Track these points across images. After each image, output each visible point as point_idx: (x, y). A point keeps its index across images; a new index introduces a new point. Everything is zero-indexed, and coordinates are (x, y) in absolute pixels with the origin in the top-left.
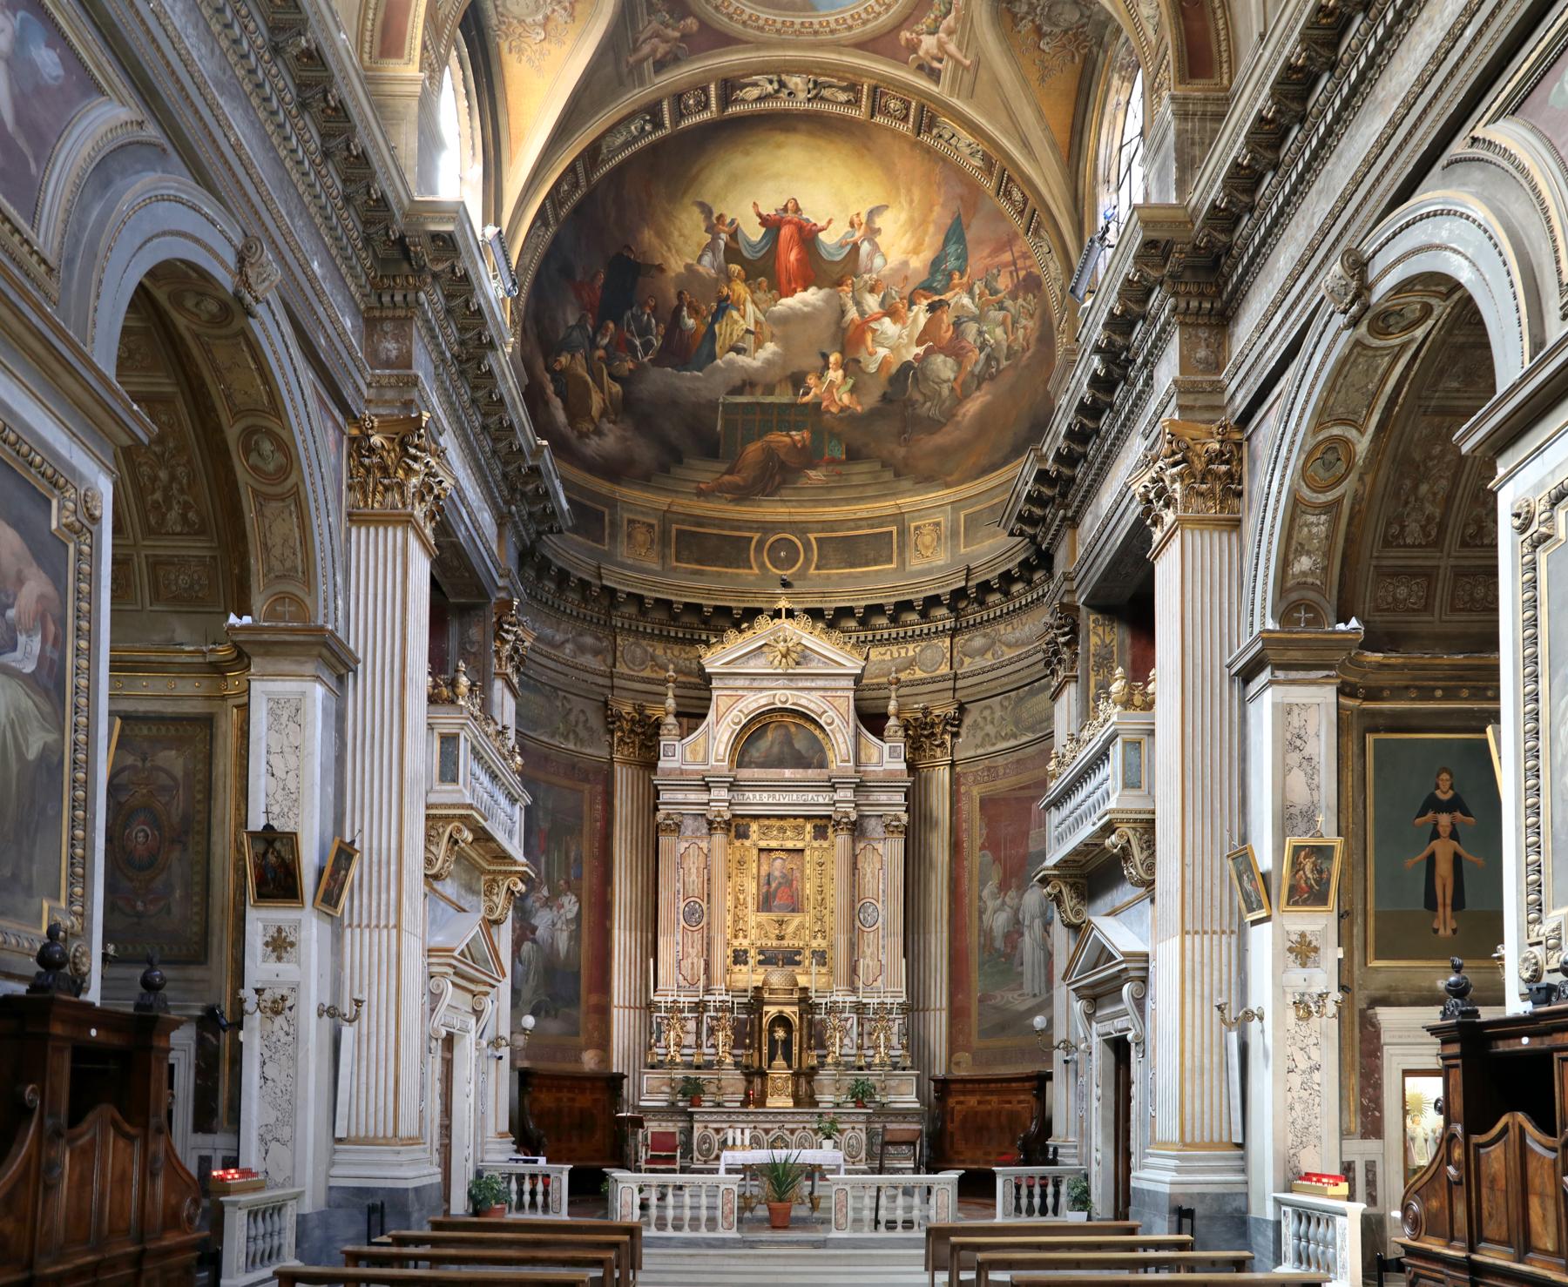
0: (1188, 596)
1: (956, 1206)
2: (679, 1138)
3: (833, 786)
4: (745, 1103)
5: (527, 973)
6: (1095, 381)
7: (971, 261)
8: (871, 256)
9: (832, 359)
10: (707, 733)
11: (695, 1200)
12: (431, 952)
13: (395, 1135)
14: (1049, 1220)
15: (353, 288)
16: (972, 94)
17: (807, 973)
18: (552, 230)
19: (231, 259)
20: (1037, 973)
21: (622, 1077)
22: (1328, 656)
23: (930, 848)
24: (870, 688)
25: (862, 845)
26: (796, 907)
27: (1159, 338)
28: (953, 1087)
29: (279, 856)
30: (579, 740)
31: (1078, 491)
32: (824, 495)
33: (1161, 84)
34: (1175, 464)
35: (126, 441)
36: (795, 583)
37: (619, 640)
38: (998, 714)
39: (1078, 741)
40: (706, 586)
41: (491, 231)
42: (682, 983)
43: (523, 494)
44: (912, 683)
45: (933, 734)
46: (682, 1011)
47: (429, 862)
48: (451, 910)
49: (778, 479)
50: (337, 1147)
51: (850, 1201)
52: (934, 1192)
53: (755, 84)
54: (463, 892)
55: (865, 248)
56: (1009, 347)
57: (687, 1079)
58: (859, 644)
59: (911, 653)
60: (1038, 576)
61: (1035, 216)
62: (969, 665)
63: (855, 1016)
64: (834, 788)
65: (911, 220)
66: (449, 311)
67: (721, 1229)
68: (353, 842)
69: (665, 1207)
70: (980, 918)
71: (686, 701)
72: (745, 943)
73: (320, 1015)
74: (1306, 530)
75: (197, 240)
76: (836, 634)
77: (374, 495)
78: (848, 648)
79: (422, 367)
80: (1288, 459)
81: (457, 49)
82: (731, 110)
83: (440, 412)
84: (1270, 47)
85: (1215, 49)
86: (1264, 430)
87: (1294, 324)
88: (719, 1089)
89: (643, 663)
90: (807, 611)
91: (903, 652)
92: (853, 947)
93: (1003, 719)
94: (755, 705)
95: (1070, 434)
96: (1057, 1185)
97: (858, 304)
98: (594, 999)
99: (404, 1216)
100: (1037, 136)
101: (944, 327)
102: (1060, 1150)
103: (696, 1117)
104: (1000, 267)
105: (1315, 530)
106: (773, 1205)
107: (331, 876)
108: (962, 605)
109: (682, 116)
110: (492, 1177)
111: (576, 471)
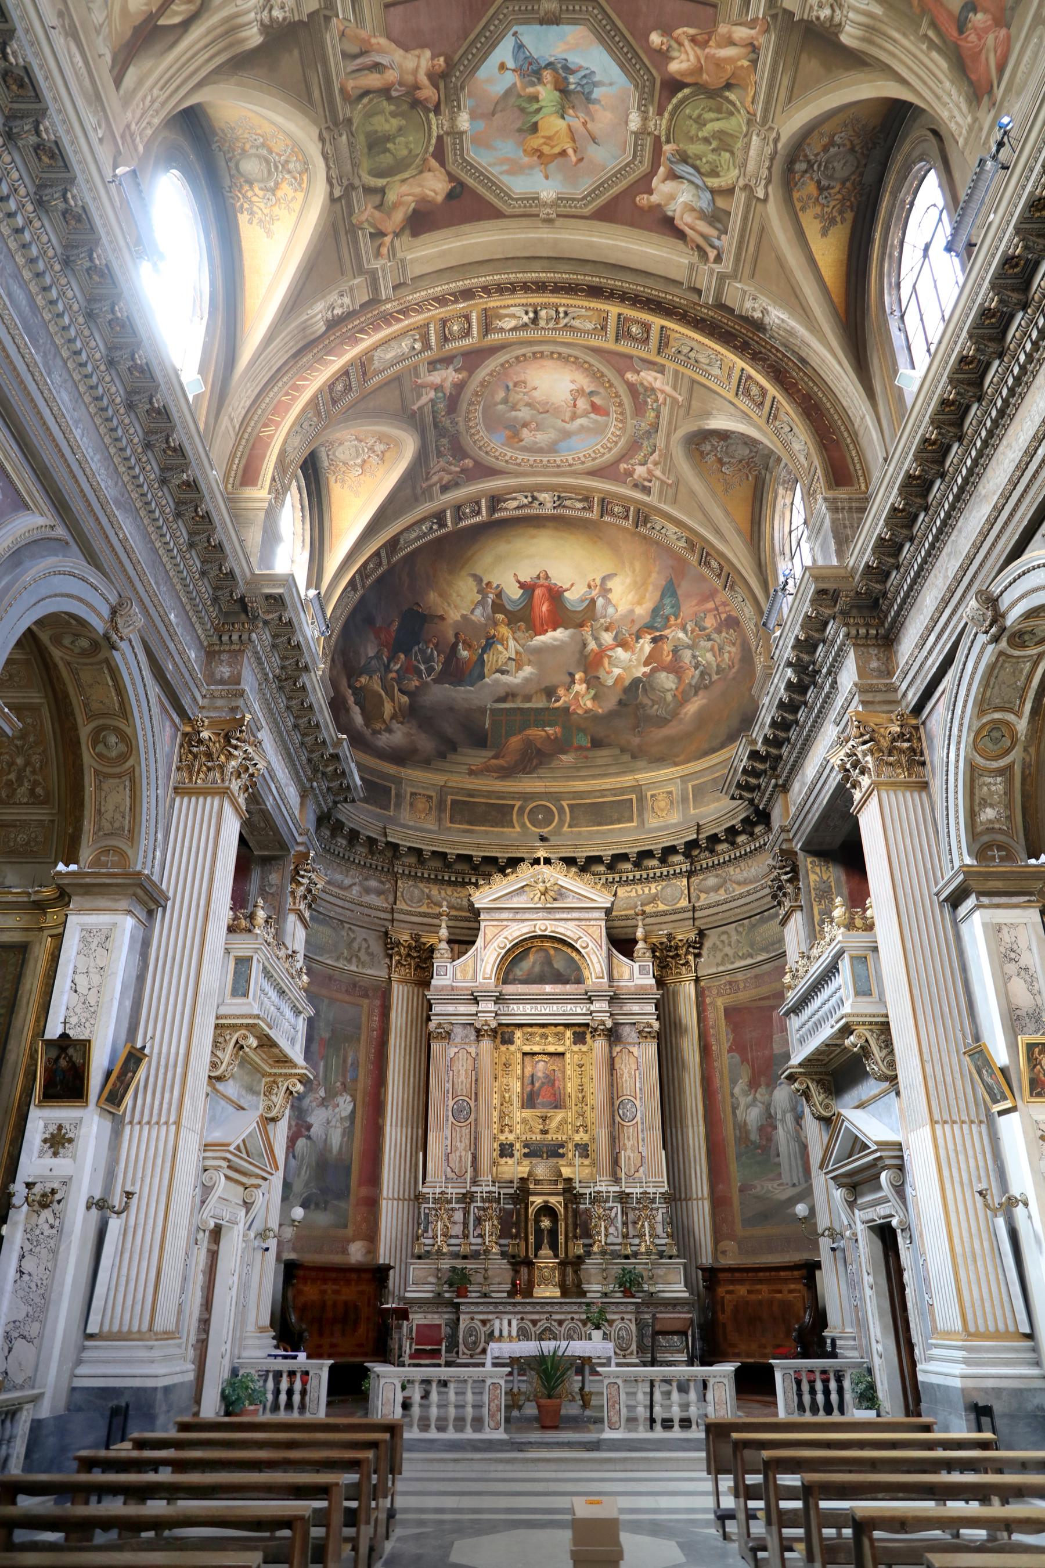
0: (892, 841)
1: (735, 1401)
2: (445, 1331)
3: (589, 998)
4: (511, 1294)
5: (300, 1168)
6: (790, 686)
7: (683, 608)
8: (605, 607)
9: (577, 677)
10: (476, 956)
11: (460, 1398)
12: (207, 1146)
14: (836, 1417)
16: (675, 501)
17: (571, 1165)
18: (359, 593)
19: (106, 612)
20: (793, 1164)
21: (388, 1268)
22: (1026, 885)
23: (682, 1051)
24: (619, 918)
25: (618, 1049)
26: (558, 1104)
27: (837, 655)
28: (722, 1276)
29: (70, 1060)
30: (361, 963)
33: (815, 491)
34: (865, 743)
37: (399, 883)
39: (809, 958)
40: (476, 841)
41: (312, 593)
42: (450, 1175)
43: (324, 774)
44: (656, 914)
45: (677, 955)
46: (449, 1202)
47: (214, 1065)
48: (231, 1109)
49: (535, 762)
50: (87, 1343)
51: (623, 1397)
52: (710, 1385)
53: (515, 499)
54: (244, 1093)
55: (600, 602)
56: (718, 666)
57: (454, 1269)
58: (607, 884)
59: (653, 891)
60: (758, 829)
61: (729, 577)
62: (704, 899)
63: (619, 1206)
64: (590, 1000)
65: (635, 582)
66: (274, 646)
67: (487, 1429)
68: (144, 1048)
69: (428, 1406)
71: (458, 931)
72: (511, 1137)
73: (88, 1208)
75: (80, 600)
77: (198, 773)
78: (599, 886)
79: (249, 682)
80: (960, 737)
81: (297, 481)
82: (497, 515)
83: (260, 715)
84: (893, 464)
85: (851, 467)
86: (935, 716)
87: (946, 642)
88: (485, 1279)
89: (420, 901)
90: (562, 859)
91: (646, 890)
92: (614, 1140)
94: (516, 934)
95: (774, 724)
96: (839, 1380)
98: (364, 1191)
99: (149, 1419)
100: (726, 527)
101: (665, 653)
102: (838, 1342)
103: (462, 1308)
104: (706, 612)
105: (993, 788)
106: (543, 1401)
107: (118, 1078)
108: (695, 852)
109: (460, 519)
110: (248, 1374)
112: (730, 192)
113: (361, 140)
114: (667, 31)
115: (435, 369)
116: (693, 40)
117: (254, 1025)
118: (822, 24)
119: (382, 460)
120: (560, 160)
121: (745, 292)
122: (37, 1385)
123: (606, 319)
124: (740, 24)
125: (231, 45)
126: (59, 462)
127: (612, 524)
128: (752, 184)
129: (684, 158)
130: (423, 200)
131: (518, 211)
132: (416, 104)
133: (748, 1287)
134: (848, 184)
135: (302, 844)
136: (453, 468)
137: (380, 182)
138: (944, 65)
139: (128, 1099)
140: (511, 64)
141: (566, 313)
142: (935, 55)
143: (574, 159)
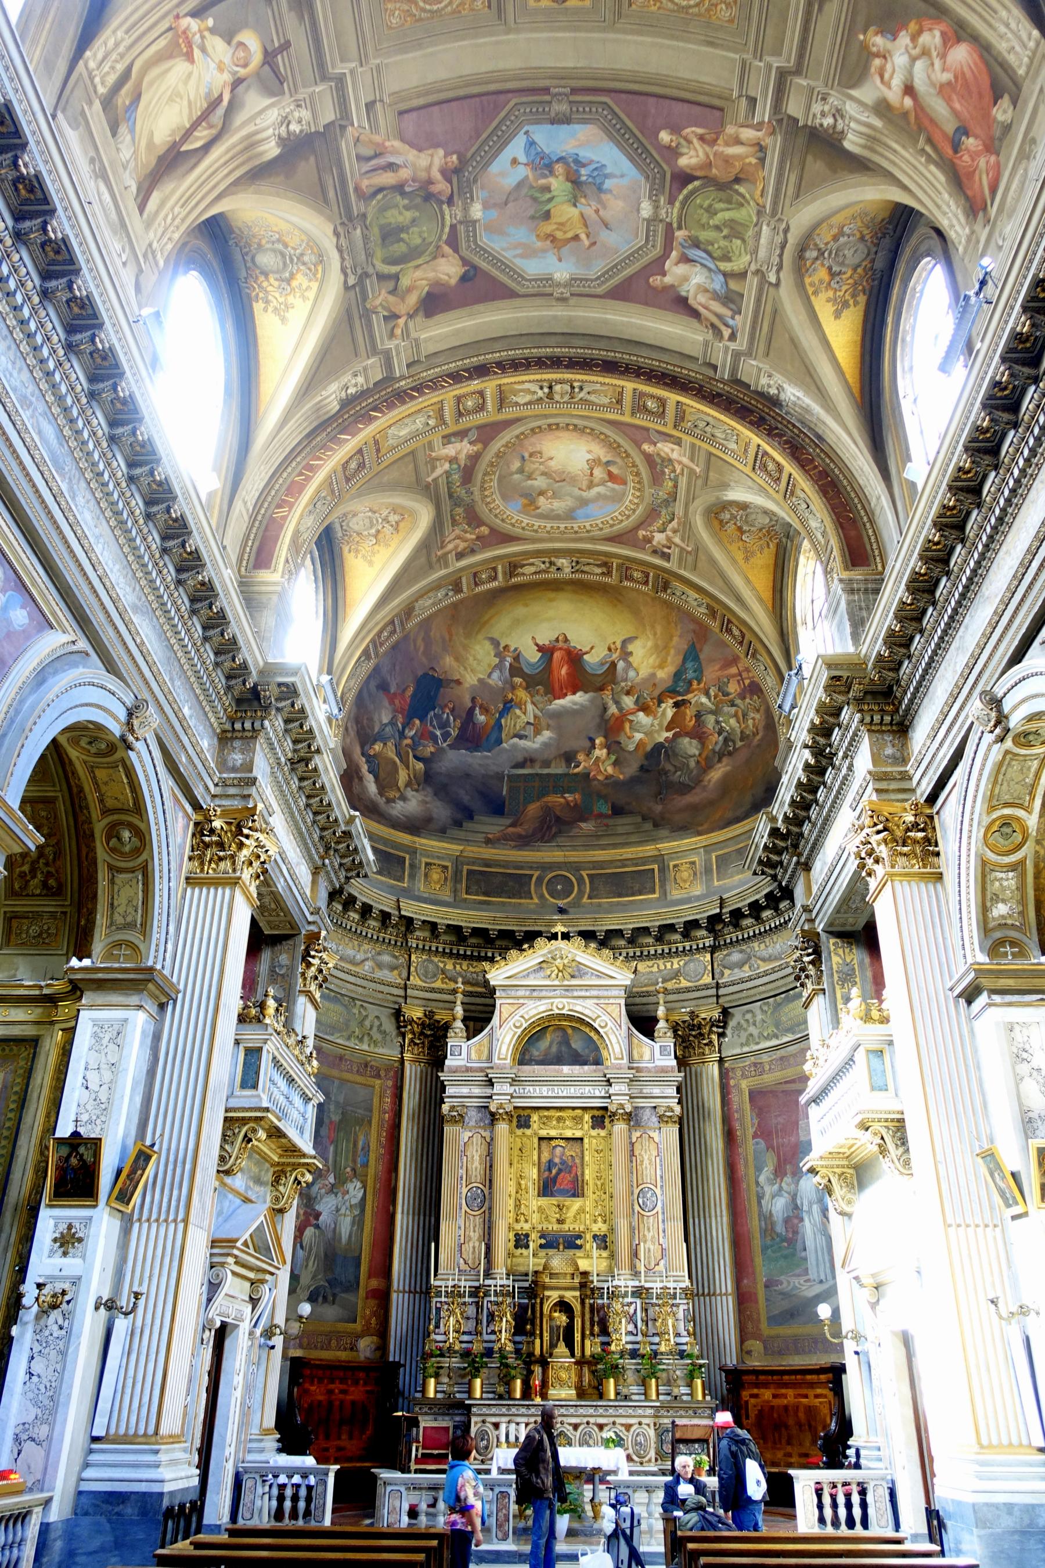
0: (905, 934)
5: (307, 1259)
6: (807, 766)
7: (705, 673)
8: (626, 671)
9: (597, 741)
10: (491, 1035)
13: (156, 1433)
15: (213, 720)
16: (695, 568)
17: (588, 1256)
19: (122, 715)
21: (397, 1365)
25: (638, 1134)
26: (576, 1190)
27: (853, 739)
28: (745, 1378)
31: (807, 842)
32: (592, 842)
34: (878, 832)
35: (17, 849)
36: (571, 910)
38: (759, 1017)
42: (463, 1267)
43: (336, 850)
44: (679, 991)
45: (701, 1034)
47: (222, 1159)
49: (554, 830)
50: (94, 1446)
53: (532, 564)
55: (621, 665)
59: (676, 966)
62: (728, 976)
67: (495, 1540)
68: (153, 1145)
70: (759, 1203)
71: (473, 1008)
72: (527, 1227)
73: (97, 1308)
74: (997, 884)
76: (606, 952)
79: (262, 768)
85: (868, 547)
91: (669, 965)
93: (764, 1021)
94: (535, 1012)
95: (793, 803)
96: (863, 1492)
97: (617, 703)
98: (374, 1283)
101: (688, 718)
102: (862, 1452)
103: (474, 1410)
104: (729, 677)
105: (1005, 883)
111: (382, 827)
112: (742, 275)
113: (375, 232)
114: (676, 130)
115: (449, 443)
116: (701, 138)
117: (261, 1118)
118: (826, 130)
119: (397, 530)
120: (573, 244)
121: (760, 370)
122: (46, 1487)
123: (621, 394)
124: (747, 126)
125: (249, 159)
126: (81, 580)
127: (632, 589)
128: (764, 268)
129: (696, 244)
130: (437, 283)
131: (531, 291)
132: (428, 197)
133: (773, 1391)
134: (859, 270)
135: (314, 923)
136: (468, 536)
137: (394, 269)
138: (942, 178)
139: (137, 1197)
140: (522, 159)
141: (581, 388)
142: (932, 168)
143: (587, 243)
